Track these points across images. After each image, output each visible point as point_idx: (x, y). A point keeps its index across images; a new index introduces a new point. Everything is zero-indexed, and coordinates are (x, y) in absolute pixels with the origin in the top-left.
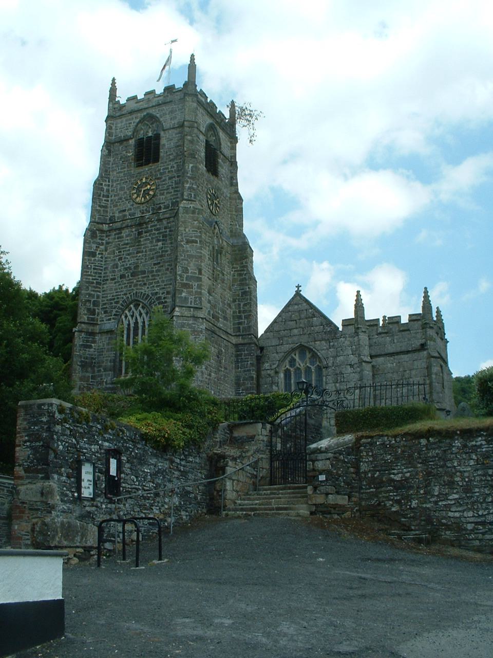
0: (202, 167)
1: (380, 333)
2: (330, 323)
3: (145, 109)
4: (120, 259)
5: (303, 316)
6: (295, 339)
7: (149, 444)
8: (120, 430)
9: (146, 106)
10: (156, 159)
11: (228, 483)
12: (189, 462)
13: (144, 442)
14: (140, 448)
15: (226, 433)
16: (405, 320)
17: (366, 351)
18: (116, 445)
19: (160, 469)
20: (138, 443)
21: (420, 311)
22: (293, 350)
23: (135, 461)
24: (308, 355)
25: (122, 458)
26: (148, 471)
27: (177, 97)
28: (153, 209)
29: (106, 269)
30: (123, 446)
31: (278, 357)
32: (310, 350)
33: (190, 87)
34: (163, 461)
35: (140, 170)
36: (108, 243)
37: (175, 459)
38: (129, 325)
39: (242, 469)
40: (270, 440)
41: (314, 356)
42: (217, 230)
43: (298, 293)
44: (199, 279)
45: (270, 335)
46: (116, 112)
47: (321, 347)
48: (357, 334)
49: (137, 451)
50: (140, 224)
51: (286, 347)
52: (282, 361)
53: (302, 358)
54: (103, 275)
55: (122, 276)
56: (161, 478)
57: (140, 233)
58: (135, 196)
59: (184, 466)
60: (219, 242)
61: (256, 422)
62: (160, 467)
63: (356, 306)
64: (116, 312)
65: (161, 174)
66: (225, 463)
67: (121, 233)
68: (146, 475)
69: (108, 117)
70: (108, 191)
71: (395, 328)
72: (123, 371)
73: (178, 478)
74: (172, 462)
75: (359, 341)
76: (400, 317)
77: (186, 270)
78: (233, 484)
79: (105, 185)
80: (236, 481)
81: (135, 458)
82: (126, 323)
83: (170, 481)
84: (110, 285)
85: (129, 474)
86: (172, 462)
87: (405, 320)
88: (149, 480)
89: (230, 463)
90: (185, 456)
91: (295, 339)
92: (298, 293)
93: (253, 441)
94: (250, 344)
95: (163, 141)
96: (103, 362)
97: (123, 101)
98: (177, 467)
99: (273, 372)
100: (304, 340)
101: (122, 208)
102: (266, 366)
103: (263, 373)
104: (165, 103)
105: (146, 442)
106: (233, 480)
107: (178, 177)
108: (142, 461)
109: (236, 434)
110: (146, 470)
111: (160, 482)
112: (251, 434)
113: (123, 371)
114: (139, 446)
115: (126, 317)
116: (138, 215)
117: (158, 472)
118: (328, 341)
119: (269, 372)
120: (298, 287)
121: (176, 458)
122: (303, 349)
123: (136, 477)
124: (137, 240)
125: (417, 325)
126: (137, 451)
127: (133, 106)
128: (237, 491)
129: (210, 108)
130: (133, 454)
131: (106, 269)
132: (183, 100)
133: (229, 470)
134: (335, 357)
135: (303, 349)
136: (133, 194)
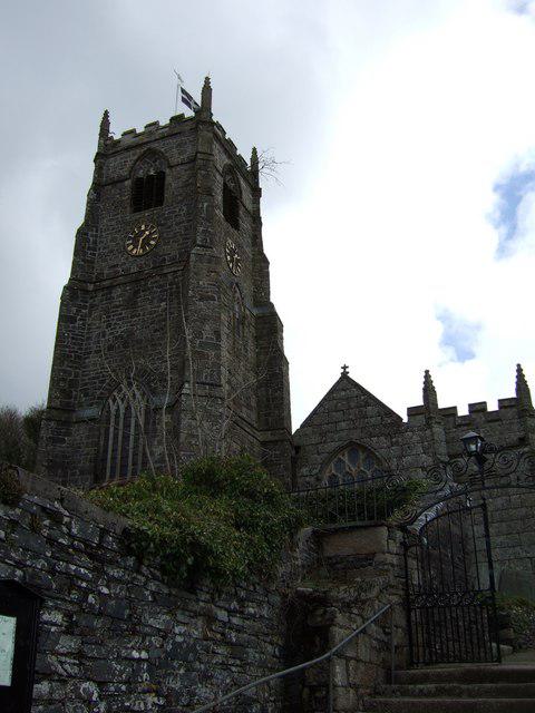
0: (219, 213)
1: (460, 425)
2: (390, 413)
3: (146, 143)
4: (109, 326)
5: (353, 405)
6: (344, 434)
7: (148, 566)
8: (44, 509)
9: (146, 140)
10: (160, 202)
11: (338, 669)
12: (252, 617)
13: (131, 561)
14: (118, 581)
15: (310, 549)
16: (493, 407)
17: (443, 449)
18: (19, 565)
19: (180, 644)
20: (112, 562)
21: (513, 395)
22: (341, 449)
23: (97, 623)
24: (362, 456)
25: (46, 617)
26: (144, 655)
27: (187, 127)
28: (154, 262)
29: (89, 338)
30: (52, 571)
31: (319, 459)
32: (365, 449)
33: (204, 115)
34: (187, 621)
35: (137, 215)
36: (92, 306)
37: (219, 613)
38: (118, 410)
39: (364, 631)
40: (403, 563)
41: (370, 454)
42: (238, 295)
43: (345, 376)
44: (218, 347)
45: (309, 430)
46: (108, 150)
47: (380, 444)
48: (429, 426)
49: (105, 591)
50: (137, 281)
51: (332, 446)
52: (325, 464)
53: (353, 460)
54: (84, 347)
55: (110, 348)
56: (182, 671)
57: (136, 292)
58: (131, 247)
59: (239, 630)
60: (240, 308)
61: (376, 526)
62: (179, 639)
63: (425, 390)
64: (102, 393)
65: (165, 219)
66: (327, 617)
67: (111, 293)
68: (136, 673)
69: (97, 154)
70: (95, 242)
71: (480, 418)
72: (108, 474)
73: (225, 666)
74: (210, 619)
75: (432, 435)
76: (485, 403)
77: (198, 334)
78: (347, 670)
79: (92, 236)
80: (352, 663)
81: (100, 614)
82: (113, 408)
83: (206, 677)
84: (93, 359)
85: (70, 676)
86: (210, 619)
87: (493, 407)
88: (144, 686)
89: (340, 618)
90: (241, 601)
91: (344, 434)
92: (345, 376)
93: (370, 564)
94: (282, 441)
95: (169, 179)
96: (80, 462)
97: (117, 137)
98: (223, 634)
99: (313, 479)
100: (355, 436)
101: (111, 263)
102: (304, 470)
103: (299, 480)
104: (171, 135)
105: (139, 561)
106: (348, 659)
107: (189, 221)
108: (126, 624)
109: (330, 551)
110: (135, 654)
111: (176, 685)
112: (365, 552)
113: (108, 474)
114: (115, 572)
115: (114, 400)
116: (134, 269)
117: (172, 655)
118: (388, 436)
119: (307, 479)
120: (345, 367)
121: (221, 608)
122: (353, 447)
123: (101, 684)
124: (131, 303)
125: (511, 413)
126: (105, 591)
127: (130, 140)
128: (356, 687)
129: (229, 148)
130: (91, 598)
131: (89, 338)
132: (195, 130)
133: (340, 634)
134: (400, 457)
135: (353, 447)
136: (128, 245)
